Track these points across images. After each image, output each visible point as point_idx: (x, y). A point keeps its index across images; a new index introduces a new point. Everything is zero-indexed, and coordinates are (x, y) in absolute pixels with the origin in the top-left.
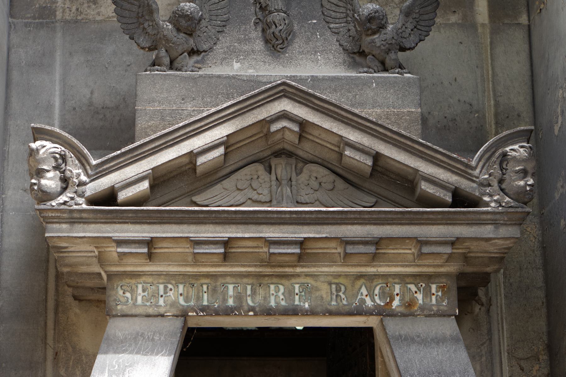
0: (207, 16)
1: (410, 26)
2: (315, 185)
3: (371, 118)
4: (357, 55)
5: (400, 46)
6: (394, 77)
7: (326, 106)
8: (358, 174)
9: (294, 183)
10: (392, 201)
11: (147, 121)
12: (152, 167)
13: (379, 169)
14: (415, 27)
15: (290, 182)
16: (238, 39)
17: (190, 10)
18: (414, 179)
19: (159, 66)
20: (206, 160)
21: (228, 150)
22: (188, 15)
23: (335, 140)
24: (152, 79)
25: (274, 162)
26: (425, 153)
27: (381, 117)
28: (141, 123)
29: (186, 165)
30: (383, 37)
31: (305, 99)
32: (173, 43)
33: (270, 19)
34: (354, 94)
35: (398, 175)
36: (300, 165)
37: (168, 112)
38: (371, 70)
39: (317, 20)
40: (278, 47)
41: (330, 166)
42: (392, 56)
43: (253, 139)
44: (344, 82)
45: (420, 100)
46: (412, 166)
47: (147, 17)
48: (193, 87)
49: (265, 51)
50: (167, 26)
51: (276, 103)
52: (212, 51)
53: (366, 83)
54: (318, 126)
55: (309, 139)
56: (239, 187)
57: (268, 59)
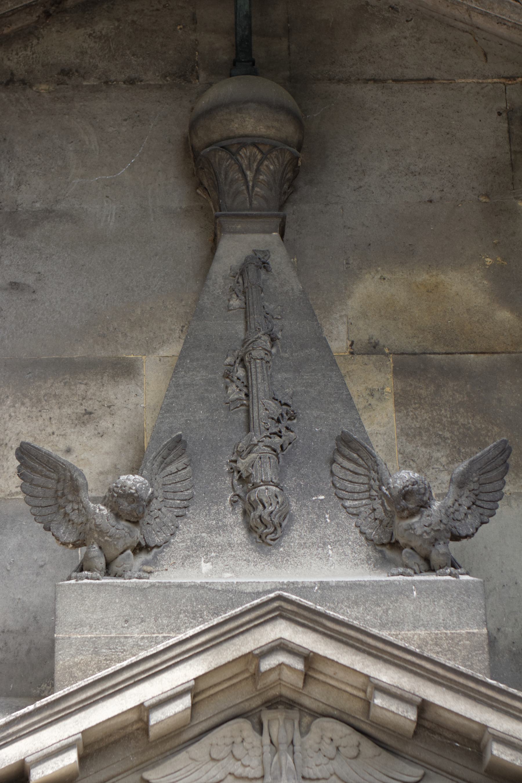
0: (160, 493)
1: (466, 502)
2: (330, 750)
3: (412, 648)
4: (388, 548)
5: (452, 533)
6: (445, 581)
7: (344, 630)
8: (394, 732)
9: (297, 748)
10: (448, 773)
11: (73, 656)
12: (82, 729)
13: (426, 724)
14: (474, 504)
15: (291, 747)
16: (208, 527)
17: (135, 485)
18: (481, 739)
19: (89, 570)
20: (163, 717)
21: (197, 699)
22: (132, 494)
23: (359, 682)
24: (80, 592)
25: (267, 716)
26: (497, 700)
27: (427, 643)
28: (63, 659)
29: (132, 724)
30: (426, 520)
31: (312, 620)
32: (110, 537)
33: (254, 496)
34: (384, 607)
35: (456, 732)
36: (306, 719)
37: (103, 642)
38: (409, 570)
39: (326, 495)
40: (268, 537)
41: (352, 721)
42: (441, 548)
43: (235, 681)
44: (368, 589)
45: (485, 615)
46: (477, 719)
47: (70, 497)
48: (141, 603)
49: (248, 545)
50: (100, 510)
51: (268, 628)
52: (168, 546)
53: (402, 591)
54: (333, 661)
55: (318, 680)
56: (214, 756)
57: (254, 556)
